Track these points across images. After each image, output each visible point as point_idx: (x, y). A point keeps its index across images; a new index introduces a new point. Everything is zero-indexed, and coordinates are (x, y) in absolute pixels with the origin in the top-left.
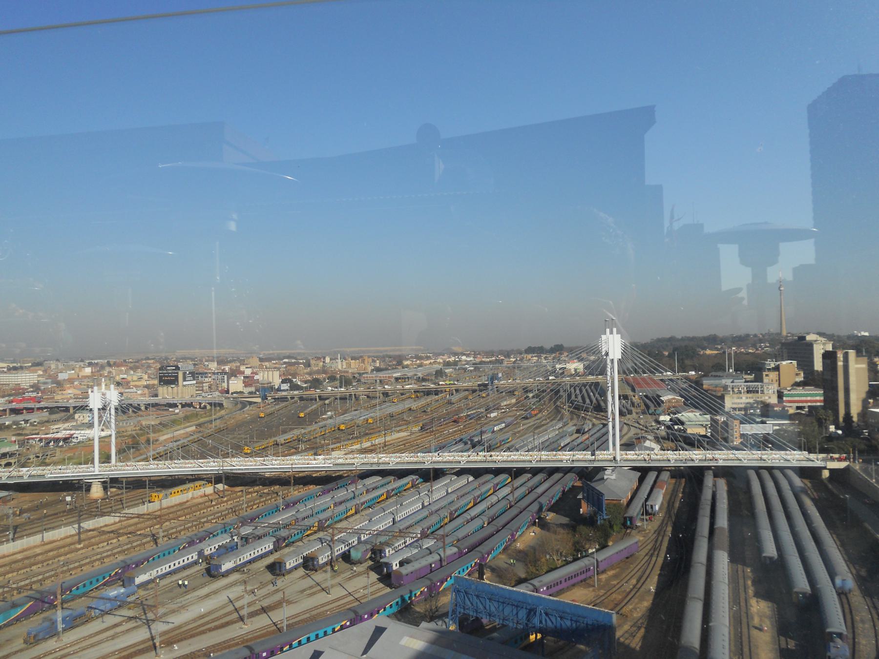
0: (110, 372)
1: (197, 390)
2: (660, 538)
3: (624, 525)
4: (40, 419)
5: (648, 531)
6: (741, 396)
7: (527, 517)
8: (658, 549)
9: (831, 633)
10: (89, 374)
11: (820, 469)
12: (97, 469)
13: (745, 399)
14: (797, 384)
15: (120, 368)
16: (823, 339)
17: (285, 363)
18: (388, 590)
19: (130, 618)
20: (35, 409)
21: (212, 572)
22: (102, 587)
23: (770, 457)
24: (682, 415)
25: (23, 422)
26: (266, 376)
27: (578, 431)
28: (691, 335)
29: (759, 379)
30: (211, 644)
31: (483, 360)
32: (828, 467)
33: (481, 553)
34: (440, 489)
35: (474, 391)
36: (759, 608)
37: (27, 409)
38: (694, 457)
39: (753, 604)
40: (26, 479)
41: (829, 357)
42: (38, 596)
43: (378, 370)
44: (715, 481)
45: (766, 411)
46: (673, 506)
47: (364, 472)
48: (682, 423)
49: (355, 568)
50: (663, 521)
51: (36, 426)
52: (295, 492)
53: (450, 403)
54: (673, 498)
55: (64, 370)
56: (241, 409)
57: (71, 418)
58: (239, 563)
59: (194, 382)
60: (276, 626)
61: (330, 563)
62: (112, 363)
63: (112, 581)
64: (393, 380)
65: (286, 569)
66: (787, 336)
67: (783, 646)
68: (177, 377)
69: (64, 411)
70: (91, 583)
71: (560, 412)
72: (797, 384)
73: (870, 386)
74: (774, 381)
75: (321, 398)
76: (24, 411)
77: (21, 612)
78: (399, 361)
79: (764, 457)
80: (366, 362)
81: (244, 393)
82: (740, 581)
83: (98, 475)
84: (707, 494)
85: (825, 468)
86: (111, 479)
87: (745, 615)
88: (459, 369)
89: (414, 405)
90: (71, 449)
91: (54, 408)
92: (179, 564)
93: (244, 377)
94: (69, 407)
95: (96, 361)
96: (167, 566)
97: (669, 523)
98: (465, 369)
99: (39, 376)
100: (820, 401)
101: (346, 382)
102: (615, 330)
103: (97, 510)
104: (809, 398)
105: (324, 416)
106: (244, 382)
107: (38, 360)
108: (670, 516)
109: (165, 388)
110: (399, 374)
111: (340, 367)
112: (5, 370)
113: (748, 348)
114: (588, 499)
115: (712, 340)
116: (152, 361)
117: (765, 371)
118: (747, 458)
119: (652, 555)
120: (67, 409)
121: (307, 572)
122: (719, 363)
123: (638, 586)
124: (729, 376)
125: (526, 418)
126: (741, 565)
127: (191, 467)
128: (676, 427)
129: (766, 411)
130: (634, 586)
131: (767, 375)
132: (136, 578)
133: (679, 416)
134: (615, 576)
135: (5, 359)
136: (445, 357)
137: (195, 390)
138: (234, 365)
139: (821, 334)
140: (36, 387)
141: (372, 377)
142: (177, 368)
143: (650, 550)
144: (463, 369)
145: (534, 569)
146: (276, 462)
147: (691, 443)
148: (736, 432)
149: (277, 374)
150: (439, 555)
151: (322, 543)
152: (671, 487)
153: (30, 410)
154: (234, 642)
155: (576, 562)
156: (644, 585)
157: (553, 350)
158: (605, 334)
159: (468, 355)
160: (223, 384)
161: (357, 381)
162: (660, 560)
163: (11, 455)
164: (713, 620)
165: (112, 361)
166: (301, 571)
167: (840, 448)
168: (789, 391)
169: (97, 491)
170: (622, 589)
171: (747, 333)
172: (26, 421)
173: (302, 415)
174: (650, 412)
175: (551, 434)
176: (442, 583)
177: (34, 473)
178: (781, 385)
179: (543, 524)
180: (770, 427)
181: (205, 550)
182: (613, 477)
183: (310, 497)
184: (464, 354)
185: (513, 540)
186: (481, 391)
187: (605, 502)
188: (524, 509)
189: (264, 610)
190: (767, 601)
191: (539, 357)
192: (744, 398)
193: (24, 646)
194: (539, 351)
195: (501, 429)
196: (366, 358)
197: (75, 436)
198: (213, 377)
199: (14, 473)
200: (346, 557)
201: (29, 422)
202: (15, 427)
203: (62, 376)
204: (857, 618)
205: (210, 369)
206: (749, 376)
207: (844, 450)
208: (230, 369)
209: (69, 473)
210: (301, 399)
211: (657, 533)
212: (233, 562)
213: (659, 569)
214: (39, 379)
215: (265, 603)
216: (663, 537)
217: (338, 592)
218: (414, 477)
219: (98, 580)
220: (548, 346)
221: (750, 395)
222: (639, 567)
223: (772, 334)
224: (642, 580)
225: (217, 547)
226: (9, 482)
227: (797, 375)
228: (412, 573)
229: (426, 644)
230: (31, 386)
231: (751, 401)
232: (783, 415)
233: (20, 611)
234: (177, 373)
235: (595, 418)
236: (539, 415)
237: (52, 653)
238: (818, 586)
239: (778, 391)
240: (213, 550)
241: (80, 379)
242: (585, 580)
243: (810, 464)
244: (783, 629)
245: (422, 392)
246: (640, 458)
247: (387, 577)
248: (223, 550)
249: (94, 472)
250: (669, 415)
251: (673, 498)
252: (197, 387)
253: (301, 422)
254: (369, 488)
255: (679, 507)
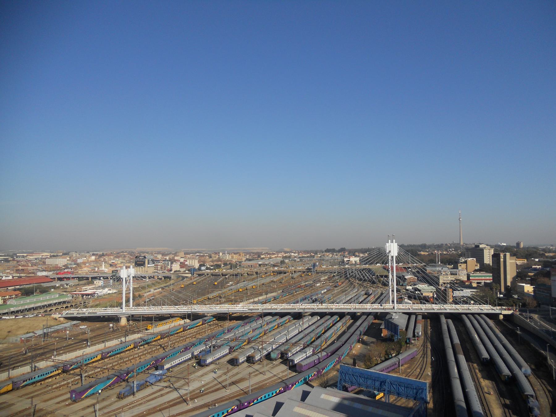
0: (104, 259)
1: (155, 270)
2: (425, 349)
3: (406, 342)
4: (75, 284)
5: (418, 345)
6: (448, 276)
7: (355, 337)
8: (426, 354)
9: (527, 395)
10: (94, 260)
11: (498, 315)
12: (124, 310)
13: (450, 278)
14: (476, 271)
15: (110, 257)
16: (489, 247)
17: (198, 256)
18: (294, 374)
19: (166, 387)
20: (71, 278)
21: (201, 363)
22: (146, 371)
23: (473, 308)
24: (418, 286)
25: (65, 285)
26: (191, 262)
27: (366, 294)
28: (412, 244)
29: (456, 267)
30: (214, 399)
31: (303, 255)
32: (502, 313)
33: (338, 355)
34: (306, 322)
35: (304, 272)
36: (486, 383)
37: (66, 278)
38: (434, 307)
39: (482, 381)
40: (87, 315)
41: (496, 257)
42: (118, 374)
43: (250, 260)
44: (447, 320)
45: (462, 285)
46: (427, 333)
47: (216, 314)
48: (420, 291)
49: (274, 362)
50: (424, 340)
51: (73, 287)
52: (234, 323)
53: (292, 278)
54: (426, 329)
55: (80, 257)
56: (182, 280)
57: (92, 283)
58: (214, 359)
59: (154, 265)
60: (243, 390)
61: (259, 360)
62: (105, 254)
63: (151, 367)
64: (258, 265)
65: (239, 362)
66: (463, 245)
67: (503, 402)
68: (144, 262)
69: (85, 279)
70: (142, 368)
71: (353, 284)
72: (476, 271)
73: (517, 272)
74: (464, 269)
75: (223, 275)
76: (65, 279)
77: (111, 382)
78: (259, 255)
79: (470, 308)
80: (241, 255)
81: (181, 271)
82: (472, 370)
83: (125, 313)
84: (445, 327)
85: (501, 314)
86: (132, 315)
87: (479, 387)
88: (292, 260)
89: (275, 279)
90: (96, 299)
91: (80, 277)
92: (179, 361)
93: (180, 263)
94: (89, 277)
95: (96, 253)
96: (178, 360)
97: (428, 342)
98: (295, 260)
99: (68, 260)
100: (489, 280)
101: (232, 266)
102: (394, 241)
103: (127, 332)
104: (477, 278)
105: (228, 284)
106: (180, 266)
107: (65, 252)
108: (427, 338)
109: (138, 268)
110: (261, 262)
111: (228, 258)
112: (49, 257)
113: (443, 251)
114: (387, 327)
115: (424, 247)
116: (126, 253)
117: (459, 264)
118: (460, 308)
119: (424, 357)
120: (87, 279)
121: (249, 364)
122: (431, 259)
123: (422, 372)
124: (439, 266)
125: (336, 287)
126: (471, 362)
127: (173, 310)
128: (417, 292)
129: (462, 285)
130: (420, 373)
131: (460, 266)
132: (165, 366)
133: (417, 286)
134: (409, 368)
135: (46, 251)
136: (283, 253)
137: (153, 269)
138: (171, 256)
139: (487, 245)
140: (66, 267)
141: (247, 264)
142: (145, 257)
143: (422, 355)
144: (294, 260)
145: (369, 363)
146: (218, 308)
147: (426, 300)
148: (450, 295)
149: (197, 261)
150: (318, 356)
151: (254, 350)
152: (423, 323)
153: (68, 279)
154: (224, 399)
155: (387, 361)
156: (424, 372)
157: (340, 251)
158: (388, 243)
159: (295, 253)
160: (168, 267)
161: (239, 266)
162: (429, 360)
163: (68, 302)
164: (467, 388)
165: (105, 253)
166: (246, 364)
167: (507, 304)
168: (473, 274)
169: (123, 322)
170: (414, 374)
171: (442, 243)
172: (67, 285)
173: (216, 283)
174: (401, 284)
175: (352, 295)
176: (323, 370)
177: (91, 311)
178: (468, 271)
179: (364, 342)
180: (467, 292)
181: (195, 352)
182: (397, 317)
183: (238, 327)
184: (293, 252)
185: (351, 349)
186: (308, 272)
187: (399, 330)
188: (353, 334)
189: (234, 383)
190: (489, 380)
191: (333, 254)
192: (449, 277)
193: (117, 399)
194: (332, 251)
195: (325, 292)
196: (241, 253)
197: (96, 293)
198: (163, 262)
199: (80, 311)
200: (268, 357)
201: (69, 284)
202: (62, 287)
203: (79, 261)
204: (535, 388)
205: (158, 258)
206: (450, 266)
207: (509, 305)
208: (169, 258)
209: (109, 312)
210: (212, 275)
211: (423, 346)
212: (211, 358)
213: (430, 364)
214: (68, 262)
215: (234, 379)
216: (427, 348)
217: (268, 375)
218: (290, 317)
219: (145, 367)
220: (337, 248)
221: (452, 276)
222: (419, 363)
223: (455, 244)
224: (423, 370)
225: (200, 351)
226: (78, 316)
227: (476, 265)
228: (307, 365)
229: (341, 399)
230: (64, 266)
231: (453, 279)
232: (470, 287)
233: (111, 381)
234: (145, 260)
235: (372, 287)
236: (342, 285)
237: (128, 405)
238: (514, 372)
239: (467, 274)
240: (198, 353)
241: (89, 262)
242: (394, 369)
243: (493, 312)
244: (501, 394)
245: (277, 272)
246: (406, 308)
247: (293, 367)
248: (204, 353)
249: (123, 311)
250: (410, 286)
251: (426, 329)
252: (154, 268)
253: (216, 287)
254: (268, 322)
255: (430, 333)
